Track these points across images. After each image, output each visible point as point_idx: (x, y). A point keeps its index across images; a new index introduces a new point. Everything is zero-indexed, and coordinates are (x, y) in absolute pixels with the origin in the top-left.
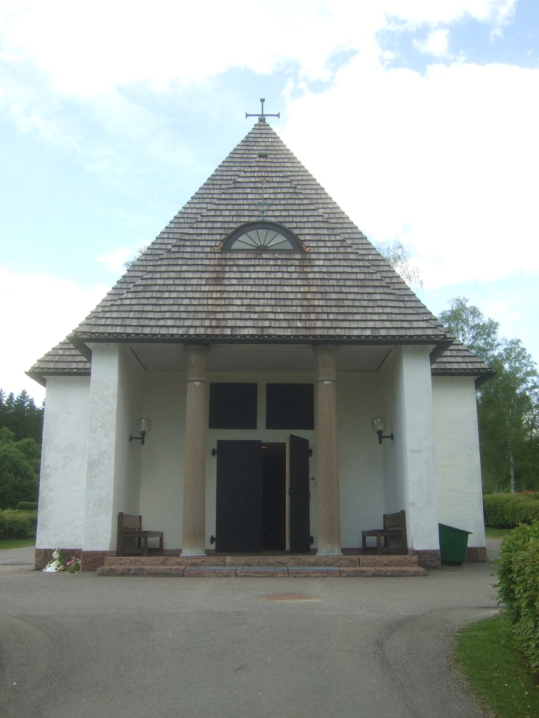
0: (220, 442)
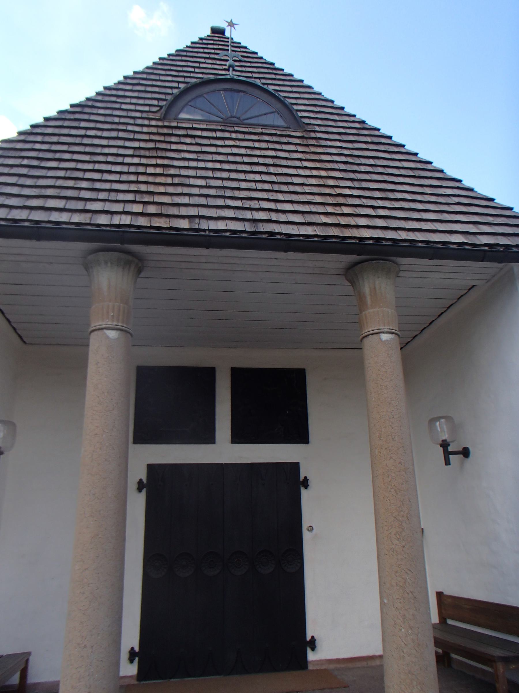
0: (151, 468)
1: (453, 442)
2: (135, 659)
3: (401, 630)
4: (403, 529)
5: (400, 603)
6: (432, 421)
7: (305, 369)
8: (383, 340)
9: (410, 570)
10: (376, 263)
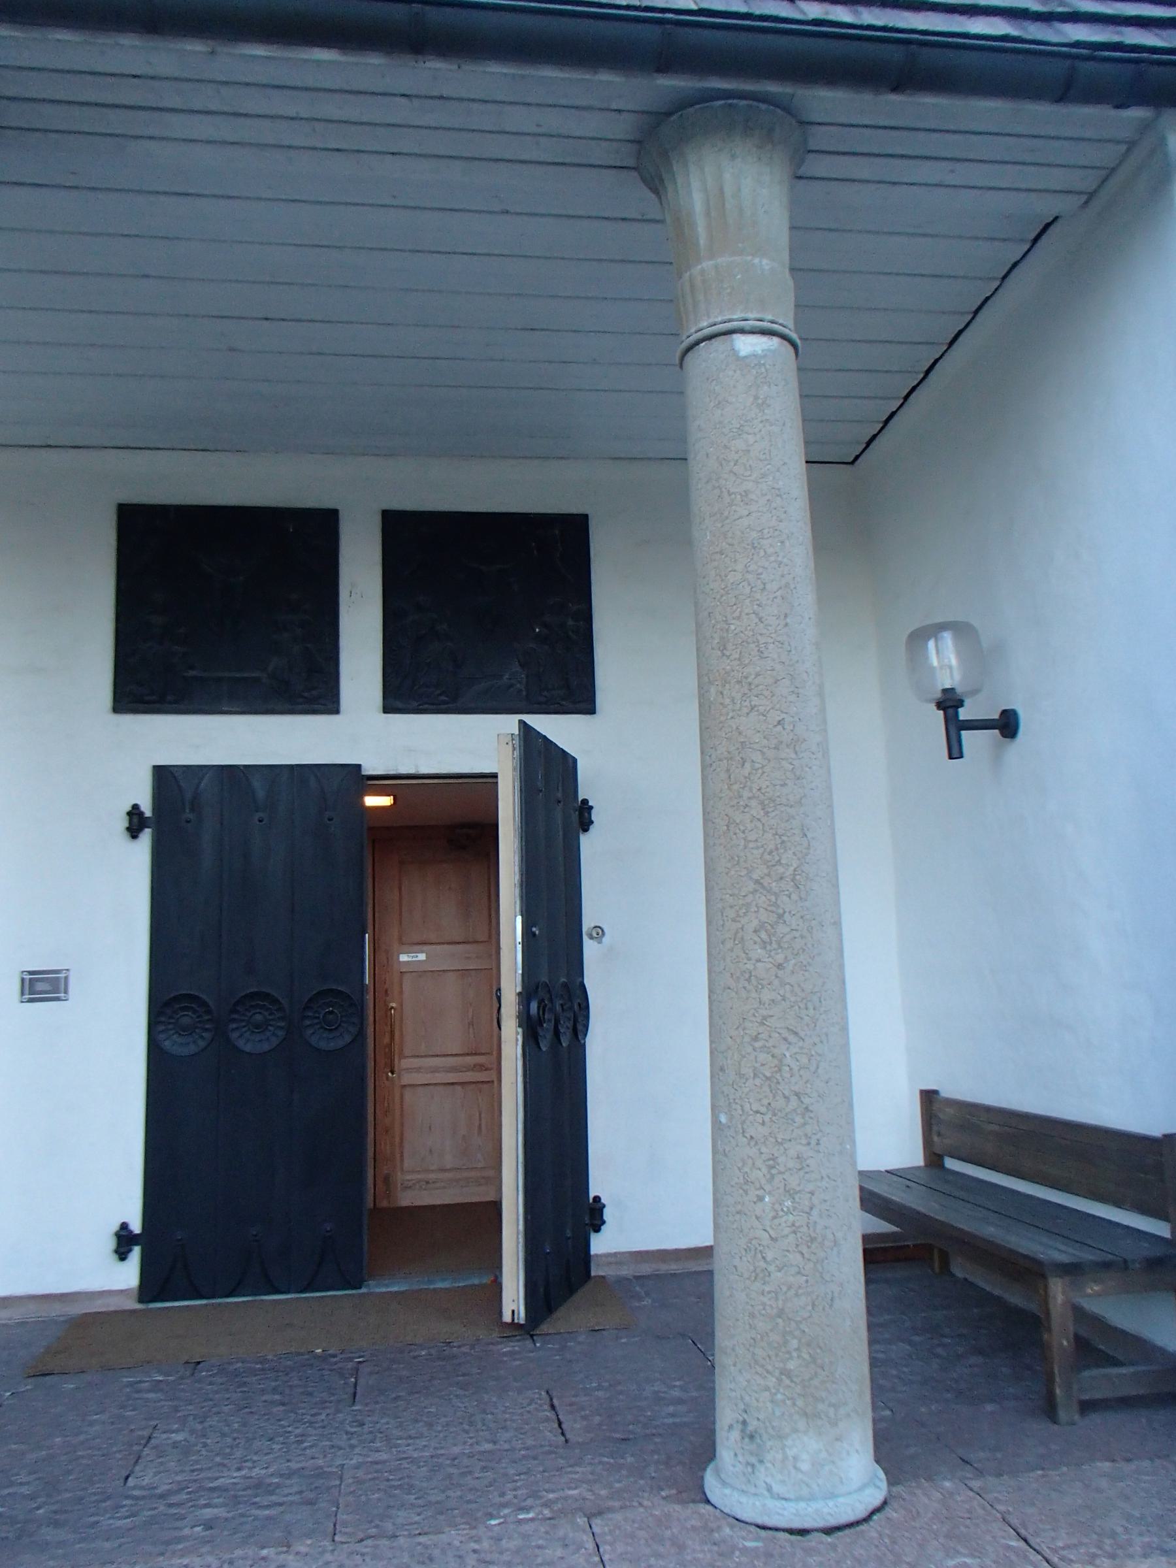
0: (163, 776)
1: (975, 692)
2: (130, 1250)
3: (761, 1199)
4: (780, 916)
5: (763, 1123)
6: (920, 637)
7: (586, 516)
8: (742, 354)
9: (796, 1033)
10: (721, 106)
